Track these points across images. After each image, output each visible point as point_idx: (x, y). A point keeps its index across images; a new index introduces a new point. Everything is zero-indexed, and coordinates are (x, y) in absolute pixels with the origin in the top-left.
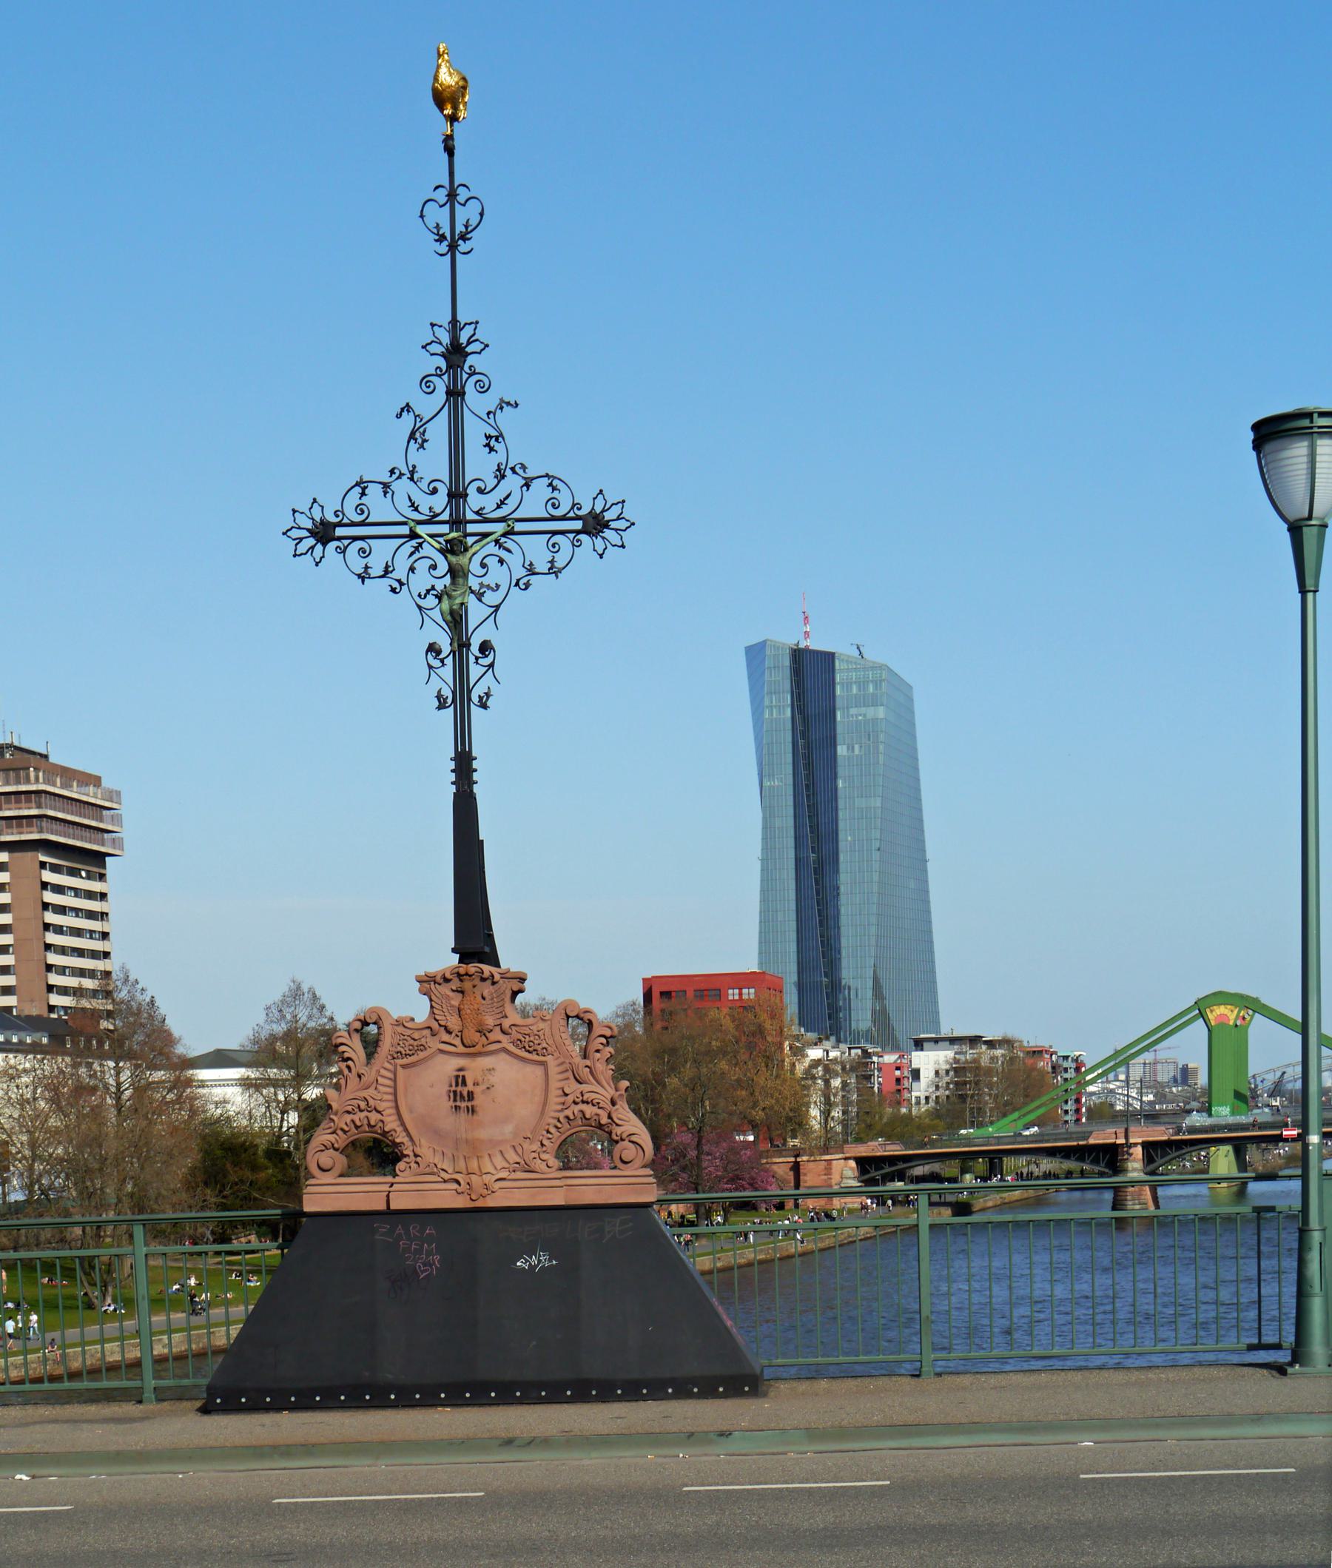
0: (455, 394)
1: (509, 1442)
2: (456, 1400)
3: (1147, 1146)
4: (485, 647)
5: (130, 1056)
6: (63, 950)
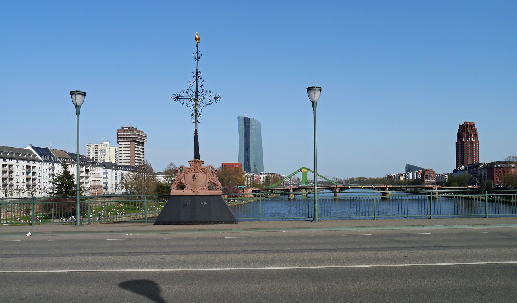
0: (197, 79)
1: (200, 230)
2: (192, 224)
3: (293, 189)
4: (200, 114)
5: (147, 172)
6: (137, 157)
